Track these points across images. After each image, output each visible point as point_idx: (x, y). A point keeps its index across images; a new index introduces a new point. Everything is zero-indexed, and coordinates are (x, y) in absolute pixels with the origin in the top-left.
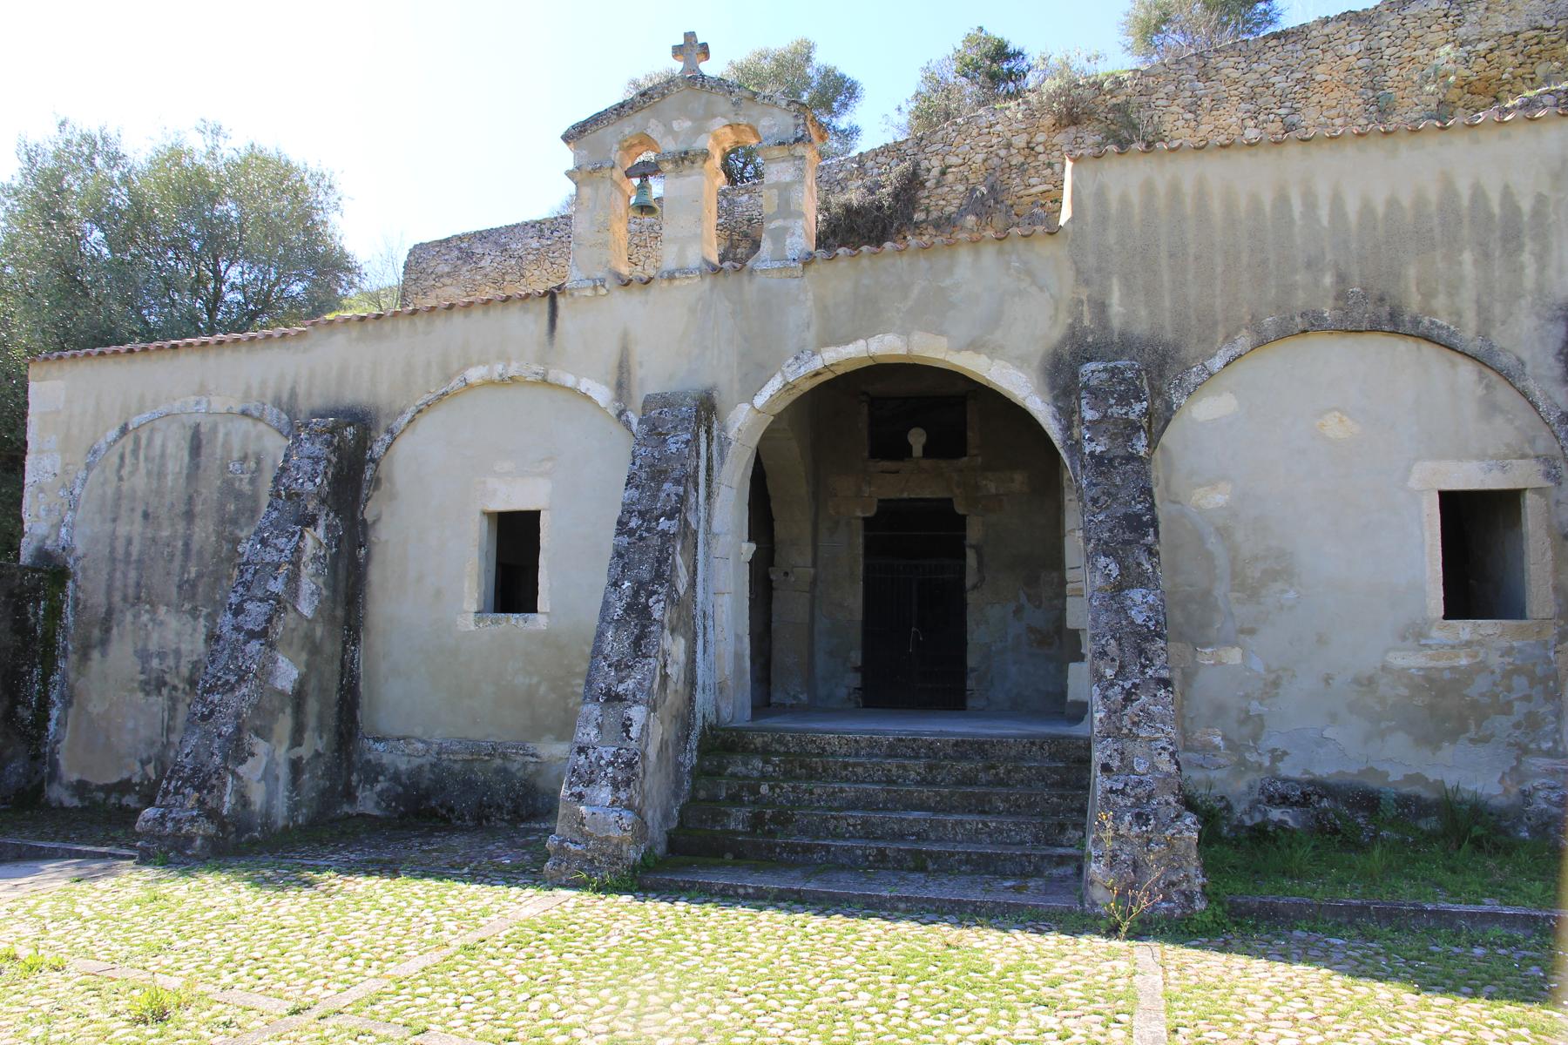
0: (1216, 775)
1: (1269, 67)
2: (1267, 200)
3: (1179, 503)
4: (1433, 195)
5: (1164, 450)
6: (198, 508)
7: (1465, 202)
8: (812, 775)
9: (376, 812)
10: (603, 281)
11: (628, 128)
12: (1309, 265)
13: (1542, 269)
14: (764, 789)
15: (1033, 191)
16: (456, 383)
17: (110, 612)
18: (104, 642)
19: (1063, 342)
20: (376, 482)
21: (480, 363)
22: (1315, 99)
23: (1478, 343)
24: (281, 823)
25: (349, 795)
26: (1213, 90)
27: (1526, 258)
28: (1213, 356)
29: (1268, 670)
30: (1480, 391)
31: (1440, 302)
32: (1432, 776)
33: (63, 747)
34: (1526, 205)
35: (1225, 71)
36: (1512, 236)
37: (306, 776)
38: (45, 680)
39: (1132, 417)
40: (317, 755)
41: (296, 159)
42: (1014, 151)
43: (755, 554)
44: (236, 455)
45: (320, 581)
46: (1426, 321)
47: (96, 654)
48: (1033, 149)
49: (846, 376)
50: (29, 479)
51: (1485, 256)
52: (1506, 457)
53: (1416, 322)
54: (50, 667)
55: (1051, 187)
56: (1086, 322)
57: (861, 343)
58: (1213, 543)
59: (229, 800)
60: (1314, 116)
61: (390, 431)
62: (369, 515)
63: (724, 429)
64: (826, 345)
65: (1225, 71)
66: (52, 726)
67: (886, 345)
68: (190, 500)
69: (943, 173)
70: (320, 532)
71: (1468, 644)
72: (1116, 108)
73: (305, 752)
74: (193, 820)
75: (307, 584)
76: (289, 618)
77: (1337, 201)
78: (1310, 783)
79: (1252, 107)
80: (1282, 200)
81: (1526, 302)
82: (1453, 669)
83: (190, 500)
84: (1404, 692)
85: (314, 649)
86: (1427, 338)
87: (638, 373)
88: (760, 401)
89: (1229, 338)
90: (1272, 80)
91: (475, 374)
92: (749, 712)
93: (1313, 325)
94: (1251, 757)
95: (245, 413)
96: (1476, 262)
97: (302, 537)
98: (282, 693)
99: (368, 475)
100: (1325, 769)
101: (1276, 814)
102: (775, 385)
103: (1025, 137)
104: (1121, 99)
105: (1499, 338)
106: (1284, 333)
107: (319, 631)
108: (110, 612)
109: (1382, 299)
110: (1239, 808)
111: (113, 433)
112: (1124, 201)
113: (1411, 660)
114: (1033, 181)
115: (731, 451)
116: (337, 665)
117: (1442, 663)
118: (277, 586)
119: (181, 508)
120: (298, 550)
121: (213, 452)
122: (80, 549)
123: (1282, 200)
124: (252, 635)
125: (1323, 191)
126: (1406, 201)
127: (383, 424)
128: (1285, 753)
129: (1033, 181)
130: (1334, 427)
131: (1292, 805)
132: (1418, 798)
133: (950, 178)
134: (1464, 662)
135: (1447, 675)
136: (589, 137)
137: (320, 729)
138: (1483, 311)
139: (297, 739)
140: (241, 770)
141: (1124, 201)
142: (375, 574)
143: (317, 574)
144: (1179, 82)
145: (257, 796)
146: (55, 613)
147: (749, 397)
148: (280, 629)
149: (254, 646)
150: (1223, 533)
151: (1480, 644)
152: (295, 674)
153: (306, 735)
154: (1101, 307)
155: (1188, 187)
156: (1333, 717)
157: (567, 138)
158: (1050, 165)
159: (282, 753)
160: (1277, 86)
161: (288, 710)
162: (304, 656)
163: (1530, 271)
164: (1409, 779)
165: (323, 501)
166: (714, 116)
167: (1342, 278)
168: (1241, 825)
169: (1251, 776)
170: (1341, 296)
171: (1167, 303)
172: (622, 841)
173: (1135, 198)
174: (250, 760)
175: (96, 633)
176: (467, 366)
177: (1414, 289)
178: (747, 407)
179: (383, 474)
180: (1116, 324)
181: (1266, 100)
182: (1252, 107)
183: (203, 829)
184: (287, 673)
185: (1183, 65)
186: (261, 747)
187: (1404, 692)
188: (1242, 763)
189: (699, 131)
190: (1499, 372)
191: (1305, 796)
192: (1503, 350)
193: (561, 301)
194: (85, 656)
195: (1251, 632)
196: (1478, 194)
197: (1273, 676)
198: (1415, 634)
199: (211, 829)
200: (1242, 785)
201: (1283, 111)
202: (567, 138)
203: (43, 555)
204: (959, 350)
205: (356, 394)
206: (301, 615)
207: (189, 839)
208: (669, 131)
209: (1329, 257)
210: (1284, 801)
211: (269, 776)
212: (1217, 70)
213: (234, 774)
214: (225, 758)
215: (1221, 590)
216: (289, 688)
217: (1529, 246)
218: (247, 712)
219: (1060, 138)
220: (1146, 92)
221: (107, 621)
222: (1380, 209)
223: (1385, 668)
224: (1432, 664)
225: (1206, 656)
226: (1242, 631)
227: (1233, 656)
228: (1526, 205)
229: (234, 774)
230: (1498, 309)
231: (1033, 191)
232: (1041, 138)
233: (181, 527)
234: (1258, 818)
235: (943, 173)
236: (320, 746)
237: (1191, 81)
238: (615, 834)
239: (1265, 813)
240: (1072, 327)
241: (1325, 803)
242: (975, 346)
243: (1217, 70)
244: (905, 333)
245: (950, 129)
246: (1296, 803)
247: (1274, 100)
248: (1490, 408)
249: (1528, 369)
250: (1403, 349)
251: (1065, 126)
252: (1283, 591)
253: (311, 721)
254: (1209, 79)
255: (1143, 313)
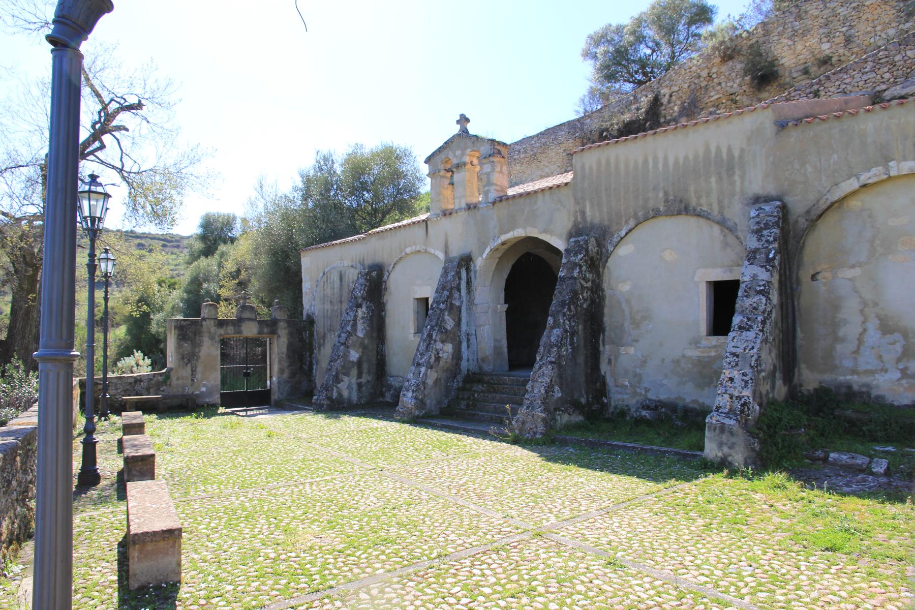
0: (625, 396)
1: (836, 4)
2: (640, 161)
3: (612, 289)
4: (701, 153)
5: (608, 268)
6: (343, 299)
7: (713, 155)
8: (495, 391)
9: (390, 401)
10: (439, 215)
11: (443, 156)
12: (654, 189)
13: (742, 182)
14: (476, 395)
15: (712, 99)
16: (403, 254)
17: (325, 334)
18: (324, 344)
19: (572, 228)
20: (386, 289)
21: (410, 246)
22: (864, 17)
23: (719, 217)
24: (355, 402)
25: (382, 395)
26: (804, 25)
27: (737, 178)
28: (621, 230)
29: (643, 356)
30: (722, 238)
31: (703, 200)
32: (701, 401)
33: (317, 378)
34: (736, 153)
35: (810, 12)
36: (730, 170)
37: (364, 388)
38: (310, 356)
39: (577, 261)
40: (368, 381)
41: (395, 145)
42: (702, 79)
43: (508, 308)
44: (351, 281)
45: (366, 325)
46: (698, 209)
47: (322, 348)
48: (711, 77)
49: (517, 242)
50: (304, 291)
51: (720, 179)
52: (732, 266)
53: (695, 210)
54: (312, 353)
55: (721, 95)
56: (579, 220)
57: (512, 232)
58: (624, 306)
59: (335, 395)
60: (863, 28)
61: (388, 271)
62: (385, 301)
63: (475, 267)
64: (501, 234)
65: (810, 12)
66: (314, 371)
67: (519, 233)
68: (341, 297)
69: (671, 96)
70: (364, 309)
71: (715, 346)
72: (751, 46)
73: (363, 380)
74: (324, 400)
75: (360, 326)
76: (354, 338)
77: (666, 159)
78: (659, 401)
79: (826, 31)
80: (646, 161)
81: (737, 198)
82: (709, 357)
83: (341, 297)
84: (690, 366)
85: (364, 347)
86: (699, 215)
87: (451, 247)
88: (484, 256)
89: (627, 222)
90: (838, 12)
91: (408, 250)
92: (507, 368)
93: (657, 214)
94: (638, 390)
95: (352, 266)
96: (717, 181)
97: (357, 311)
98: (353, 362)
99: (383, 287)
100: (663, 397)
101: (644, 413)
102: (488, 250)
103: (706, 71)
104: (754, 40)
105: (727, 214)
106: (646, 219)
107: (366, 341)
108: (325, 334)
109: (681, 201)
110: (633, 410)
111: (321, 274)
112: (591, 168)
113: (693, 353)
114: (712, 94)
115: (478, 275)
116: (375, 352)
117: (705, 355)
118: (349, 328)
119: (339, 299)
120: (355, 316)
121: (346, 279)
122: (316, 313)
123: (646, 161)
124: (342, 344)
125: (661, 156)
126: (691, 157)
127: (386, 268)
128: (649, 389)
129: (712, 94)
130: (668, 256)
131: (651, 409)
132: (696, 409)
133: (674, 98)
134: (713, 354)
135: (706, 359)
136: (432, 161)
137: (369, 373)
138: (720, 203)
139: (360, 375)
140: (339, 385)
141: (591, 168)
142: (388, 321)
143: (364, 323)
144: (785, 24)
145: (345, 394)
146: (312, 335)
147: (481, 254)
148: (350, 342)
149: (342, 347)
150: (628, 301)
151: (719, 346)
152: (357, 356)
153: (363, 375)
154: (583, 213)
155: (612, 160)
156: (666, 376)
157: (426, 162)
158: (720, 84)
159: (354, 380)
160: (842, 14)
161: (355, 367)
162: (361, 350)
163: (738, 183)
164: (694, 401)
165: (364, 299)
166: (467, 148)
167: (666, 194)
168: (633, 417)
169: (638, 398)
170: (666, 201)
171: (605, 210)
172: (412, 408)
173: (594, 167)
174: (342, 383)
175: (322, 341)
176: (406, 247)
177: (693, 195)
178: (480, 258)
179: (387, 286)
180: (589, 219)
181: (836, 24)
182: (826, 31)
183: (326, 402)
184: (354, 355)
185: (787, 14)
186: (346, 379)
187: (690, 366)
188: (635, 392)
189: (463, 154)
190: (728, 229)
191: (656, 407)
192: (729, 219)
193: (428, 222)
194: (320, 349)
195: (637, 341)
196: (718, 150)
197: (644, 359)
198: (695, 342)
199: (329, 403)
200: (634, 401)
201: (844, 29)
202: (426, 162)
203: (308, 316)
204: (541, 233)
205: (378, 259)
206: (358, 337)
207: (323, 405)
208: (455, 156)
209: (662, 185)
210: (648, 408)
211: (349, 387)
212: (806, 12)
213: (337, 387)
214: (333, 382)
215: (627, 324)
216: (355, 360)
217: (737, 172)
218: (340, 368)
219: (724, 68)
220: (767, 33)
221: (324, 337)
222: (681, 161)
223: (683, 356)
224: (701, 355)
225: (622, 350)
226: (633, 341)
227: (632, 350)
228: (736, 153)
229: (337, 387)
230: (726, 202)
231: (712, 99)
232: (714, 70)
233: (339, 305)
234: (638, 414)
235: (671, 96)
236: (369, 378)
237: (792, 22)
238: (410, 406)
239: (640, 412)
240: (574, 221)
241: (663, 410)
242: (545, 231)
243: (806, 12)
244: (524, 228)
245: (672, 73)
246: (652, 409)
247: (839, 23)
248: (726, 245)
249: (738, 228)
250: (693, 220)
251: (727, 61)
252: (648, 325)
253: (365, 370)
254: (802, 19)
255: (597, 214)
